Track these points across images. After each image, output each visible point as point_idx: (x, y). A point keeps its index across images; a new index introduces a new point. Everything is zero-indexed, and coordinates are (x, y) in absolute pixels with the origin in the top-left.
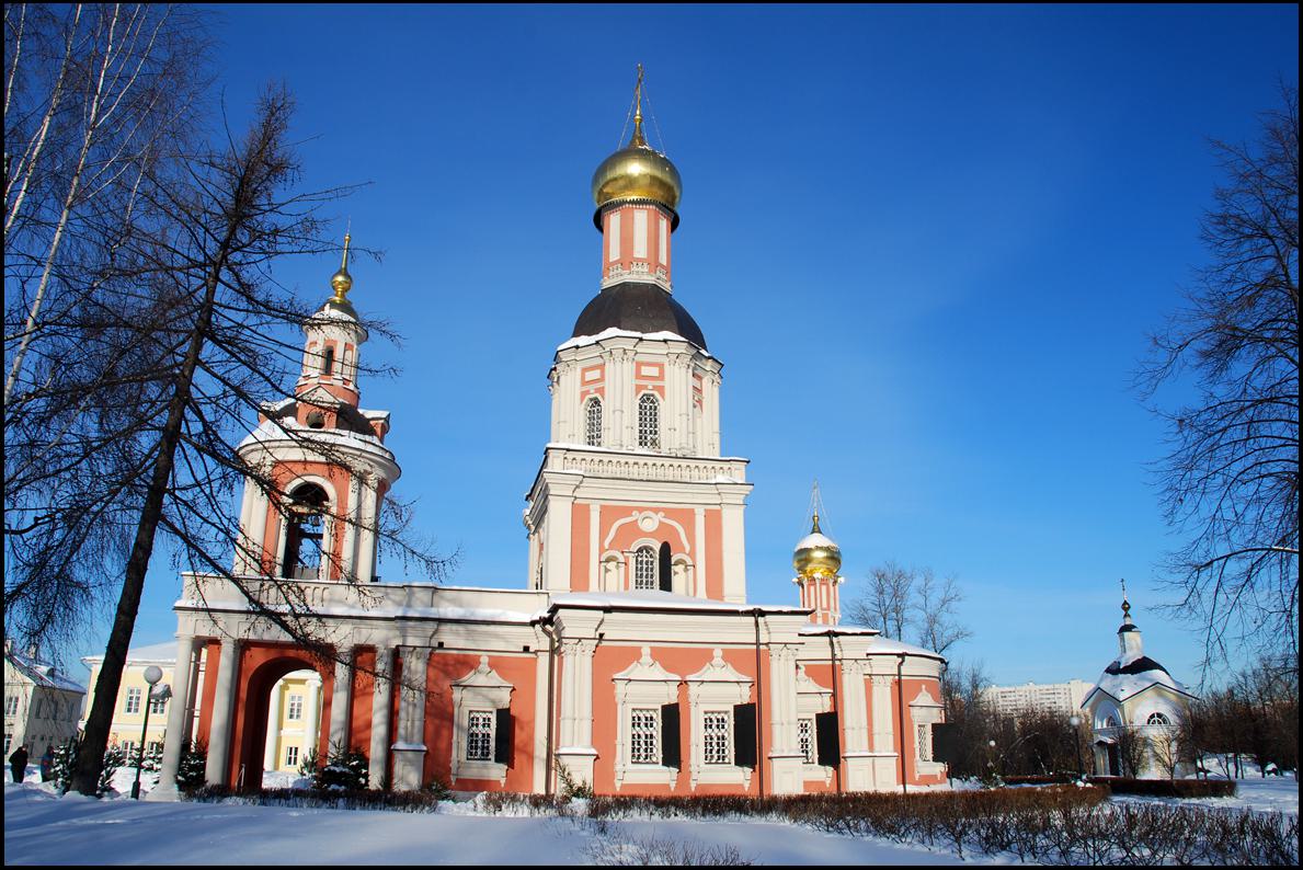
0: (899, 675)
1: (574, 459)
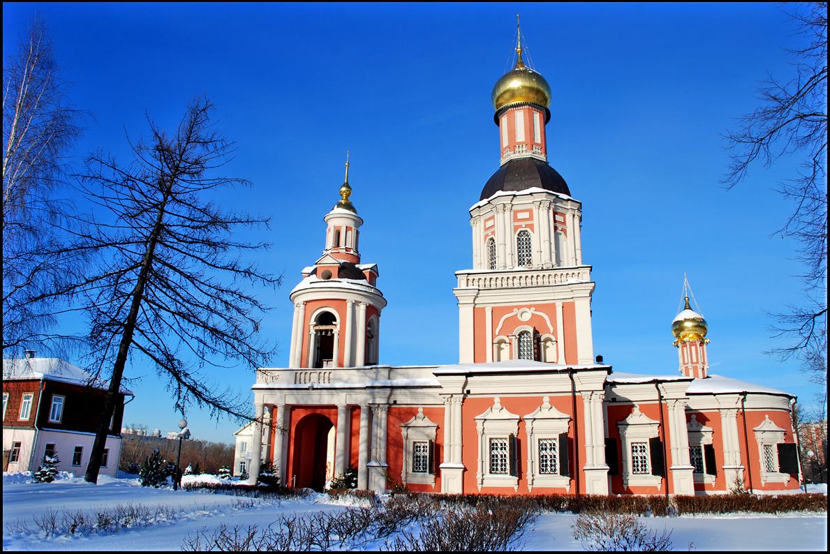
0: (743, 408)
1: (573, 274)
